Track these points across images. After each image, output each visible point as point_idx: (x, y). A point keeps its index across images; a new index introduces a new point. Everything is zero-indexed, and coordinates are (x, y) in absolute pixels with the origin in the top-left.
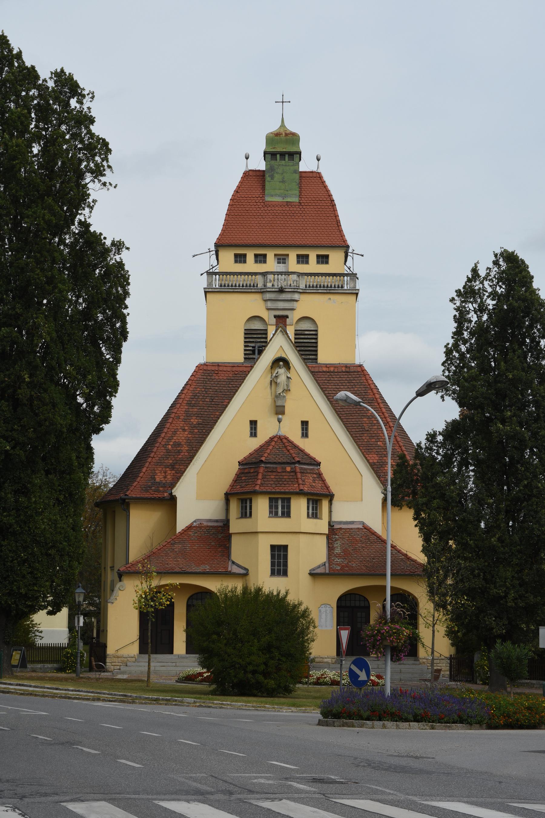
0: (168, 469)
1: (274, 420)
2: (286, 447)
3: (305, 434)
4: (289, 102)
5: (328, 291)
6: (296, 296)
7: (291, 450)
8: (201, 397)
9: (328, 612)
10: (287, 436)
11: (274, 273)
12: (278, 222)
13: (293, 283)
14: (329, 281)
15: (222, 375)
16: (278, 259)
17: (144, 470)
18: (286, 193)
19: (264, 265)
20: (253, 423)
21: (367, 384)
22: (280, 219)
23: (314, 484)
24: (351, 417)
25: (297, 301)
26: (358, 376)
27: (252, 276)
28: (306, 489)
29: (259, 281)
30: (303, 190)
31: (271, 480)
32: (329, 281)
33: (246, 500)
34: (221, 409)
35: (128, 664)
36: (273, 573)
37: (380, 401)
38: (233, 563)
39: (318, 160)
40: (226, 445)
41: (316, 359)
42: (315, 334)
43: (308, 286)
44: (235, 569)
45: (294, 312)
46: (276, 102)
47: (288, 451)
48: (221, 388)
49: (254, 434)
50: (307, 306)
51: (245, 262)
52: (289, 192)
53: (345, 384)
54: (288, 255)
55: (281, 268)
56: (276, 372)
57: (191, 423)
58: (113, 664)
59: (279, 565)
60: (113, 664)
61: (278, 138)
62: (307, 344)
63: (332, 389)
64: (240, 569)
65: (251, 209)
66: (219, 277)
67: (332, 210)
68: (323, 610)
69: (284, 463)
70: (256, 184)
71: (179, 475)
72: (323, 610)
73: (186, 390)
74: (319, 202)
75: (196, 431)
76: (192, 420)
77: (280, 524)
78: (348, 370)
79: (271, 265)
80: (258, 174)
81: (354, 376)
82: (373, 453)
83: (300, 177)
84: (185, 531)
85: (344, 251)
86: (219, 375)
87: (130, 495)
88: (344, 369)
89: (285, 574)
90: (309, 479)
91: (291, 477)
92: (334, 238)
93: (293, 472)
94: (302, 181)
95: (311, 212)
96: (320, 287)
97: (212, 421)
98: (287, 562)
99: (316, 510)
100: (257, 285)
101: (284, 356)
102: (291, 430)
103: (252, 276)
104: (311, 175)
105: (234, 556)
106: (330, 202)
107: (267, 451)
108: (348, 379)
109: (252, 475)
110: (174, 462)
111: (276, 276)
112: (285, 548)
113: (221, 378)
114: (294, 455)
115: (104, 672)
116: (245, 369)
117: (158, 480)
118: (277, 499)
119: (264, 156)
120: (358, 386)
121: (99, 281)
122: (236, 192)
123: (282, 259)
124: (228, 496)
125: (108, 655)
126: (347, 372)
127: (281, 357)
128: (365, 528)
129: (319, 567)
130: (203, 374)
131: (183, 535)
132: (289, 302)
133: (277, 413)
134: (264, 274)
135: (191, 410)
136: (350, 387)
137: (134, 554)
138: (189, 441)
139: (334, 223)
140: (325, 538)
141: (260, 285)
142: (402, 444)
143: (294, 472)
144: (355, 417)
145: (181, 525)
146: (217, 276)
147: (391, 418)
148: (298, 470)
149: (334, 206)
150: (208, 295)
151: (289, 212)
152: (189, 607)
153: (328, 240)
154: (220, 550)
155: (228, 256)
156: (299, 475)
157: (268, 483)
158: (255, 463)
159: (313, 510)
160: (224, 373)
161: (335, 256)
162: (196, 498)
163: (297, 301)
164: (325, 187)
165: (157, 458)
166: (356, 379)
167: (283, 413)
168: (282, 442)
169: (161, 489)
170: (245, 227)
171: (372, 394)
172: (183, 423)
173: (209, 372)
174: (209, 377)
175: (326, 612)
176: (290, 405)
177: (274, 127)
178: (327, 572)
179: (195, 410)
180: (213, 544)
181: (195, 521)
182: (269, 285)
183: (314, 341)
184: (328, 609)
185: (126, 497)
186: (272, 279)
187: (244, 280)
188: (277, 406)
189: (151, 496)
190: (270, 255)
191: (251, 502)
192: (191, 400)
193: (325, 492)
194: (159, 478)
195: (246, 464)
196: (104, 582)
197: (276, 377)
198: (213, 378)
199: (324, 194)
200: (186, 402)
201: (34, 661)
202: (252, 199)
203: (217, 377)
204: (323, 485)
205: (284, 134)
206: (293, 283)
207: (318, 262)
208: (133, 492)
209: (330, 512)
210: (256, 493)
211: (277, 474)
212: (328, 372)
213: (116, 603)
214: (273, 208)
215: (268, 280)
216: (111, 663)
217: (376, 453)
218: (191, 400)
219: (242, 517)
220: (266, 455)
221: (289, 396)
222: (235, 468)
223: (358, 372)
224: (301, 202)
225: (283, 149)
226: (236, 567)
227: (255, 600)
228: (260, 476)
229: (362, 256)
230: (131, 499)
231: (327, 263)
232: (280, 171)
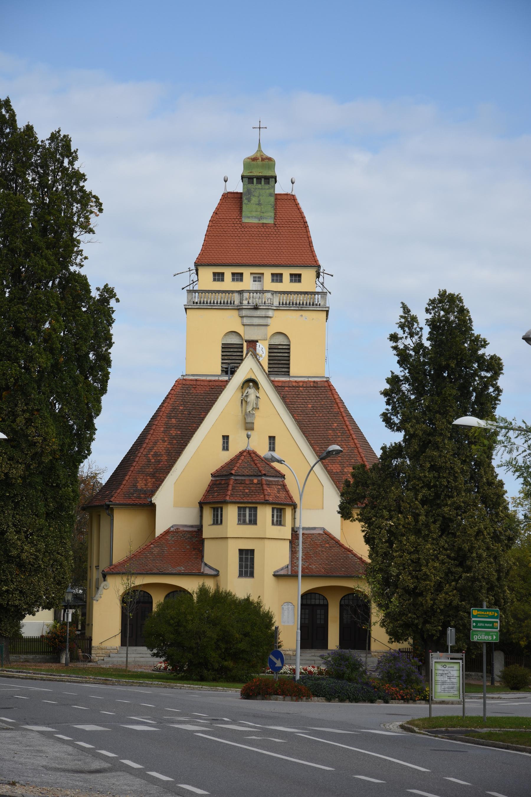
0: (148, 477)
1: (244, 433)
2: (253, 461)
3: (272, 448)
5: (300, 309)
6: (270, 313)
7: (258, 464)
10: (256, 450)
11: (249, 291)
12: (255, 243)
13: (268, 301)
14: (300, 299)
15: (200, 389)
16: (254, 277)
17: (127, 478)
18: (262, 215)
20: (226, 438)
21: (333, 398)
22: (256, 240)
23: (278, 495)
24: (317, 430)
25: (271, 317)
26: (325, 391)
27: (229, 294)
28: (271, 499)
29: (236, 298)
30: (278, 212)
31: (239, 491)
32: (300, 299)
33: (217, 508)
34: (198, 421)
35: (111, 655)
36: (241, 575)
37: (344, 415)
38: (206, 564)
40: (201, 456)
41: (289, 372)
43: (281, 304)
44: (207, 571)
45: (268, 327)
46: (253, 128)
47: (256, 465)
48: (198, 401)
49: (226, 447)
50: (282, 322)
51: (223, 280)
52: (265, 214)
54: (263, 274)
55: (255, 286)
56: (246, 392)
57: (170, 434)
61: (255, 163)
62: (280, 359)
63: (300, 403)
64: (212, 571)
65: (228, 230)
66: (198, 295)
67: (305, 231)
68: (285, 607)
69: (251, 476)
70: (234, 206)
71: (159, 482)
72: (285, 607)
73: (166, 403)
74: (293, 223)
75: (175, 442)
76: (171, 432)
77: (248, 530)
78: (315, 385)
79: (248, 283)
80: (236, 196)
81: (321, 391)
82: (336, 463)
83: (276, 199)
84: (163, 536)
85: (316, 270)
86: (197, 389)
87: (114, 502)
88: (312, 384)
89: (252, 575)
91: (257, 488)
92: (306, 258)
93: (259, 484)
94: (278, 203)
95: (286, 233)
96: (293, 304)
97: (190, 433)
98: (253, 564)
99: (280, 517)
103: (229, 294)
104: (286, 197)
105: (207, 559)
106: (303, 223)
107: (236, 465)
108: (315, 393)
109: (223, 486)
110: (155, 470)
111: (251, 294)
112: (252, 552)
113: (198, 392)
114: (261, 469)
115: (90, 662)
116: (221, 384)
117: (139, 487)
118: (245, 508)
119: (242, 179)
120: (325, 401)
121: (85, 326)
122: (215, 213)
123: (258, 278)
124: (202, 505)
125: (93, 647)
126: (315, 387)
128: (325, 534)
129: (282, 569)
131: (161, 539)
132: (264, 319)
133: (247, 429)
134: (241, 292)
139: (306, 244)
141: (237, 302)
142: (363, 455)
143: (260, 483)
144: (321, 430)
145: (160, 530)
146: (197, 294)
147: (354, 430)
148: (264, 482)
149: (306, 227)
150: (188, 310)
151: (265, 233)
152: (342, 608)
153: (301, 260)
154: (194, 553)
155: (207, 273)
156: (265, 487)
157: (237, 493)
158: (226, 475)
159: (277, 518)
160: (201, 387)
161: (308, 275)
162: (173, 504)
163: (271, 317)
164: (299, 209)
166: (323, 393)
167: (252, 429)
168: (251, 456)
169: (142, 496)
170: (223, 247)
171: (337, 408)
173: (187, 386)
174: (187, 391)
175: (288, 610)
176: (258, 422)
177: (251, 152)
178: (290, 573)
180: (188, 547)
181: (172, 527)
182: (245, 302)
183: (286, 355)
184: (290, 607)
185: (110, 503)
186: (248, 297)
187: (222, 298)
189: (133, 502)
190: (247, 272)
191: (222, 511)
192: (170, 412)
194: (141, 485)
195: (218, 476)
196: (90, 579)
197: (247, 396)
198: (191, 392)
199: (298, 216)
200: (166, 414)
203: (195, 391)
204: (287, 495)
205: (260, 159)
206: (268, 301)
207: (291, 281)
208: (117, 498)
209: (294, 519)
210: (226, 503)
211: (246, 484)
212: (297, 387)
213: (100, 600)
214: (250, 230)
215: (244, 298)
217: (340, 463)
218: (170, 412)
219: (214, 524)
221: (257, 413)
222: (210, 478)
223: (325, 387)
224: (276, 223)
225: (259, 174)
226: (208, 568)
227: (221, 600)
228: (230, 488)
229: (332, 276)
231: (300, 281)
232: (257, 194)
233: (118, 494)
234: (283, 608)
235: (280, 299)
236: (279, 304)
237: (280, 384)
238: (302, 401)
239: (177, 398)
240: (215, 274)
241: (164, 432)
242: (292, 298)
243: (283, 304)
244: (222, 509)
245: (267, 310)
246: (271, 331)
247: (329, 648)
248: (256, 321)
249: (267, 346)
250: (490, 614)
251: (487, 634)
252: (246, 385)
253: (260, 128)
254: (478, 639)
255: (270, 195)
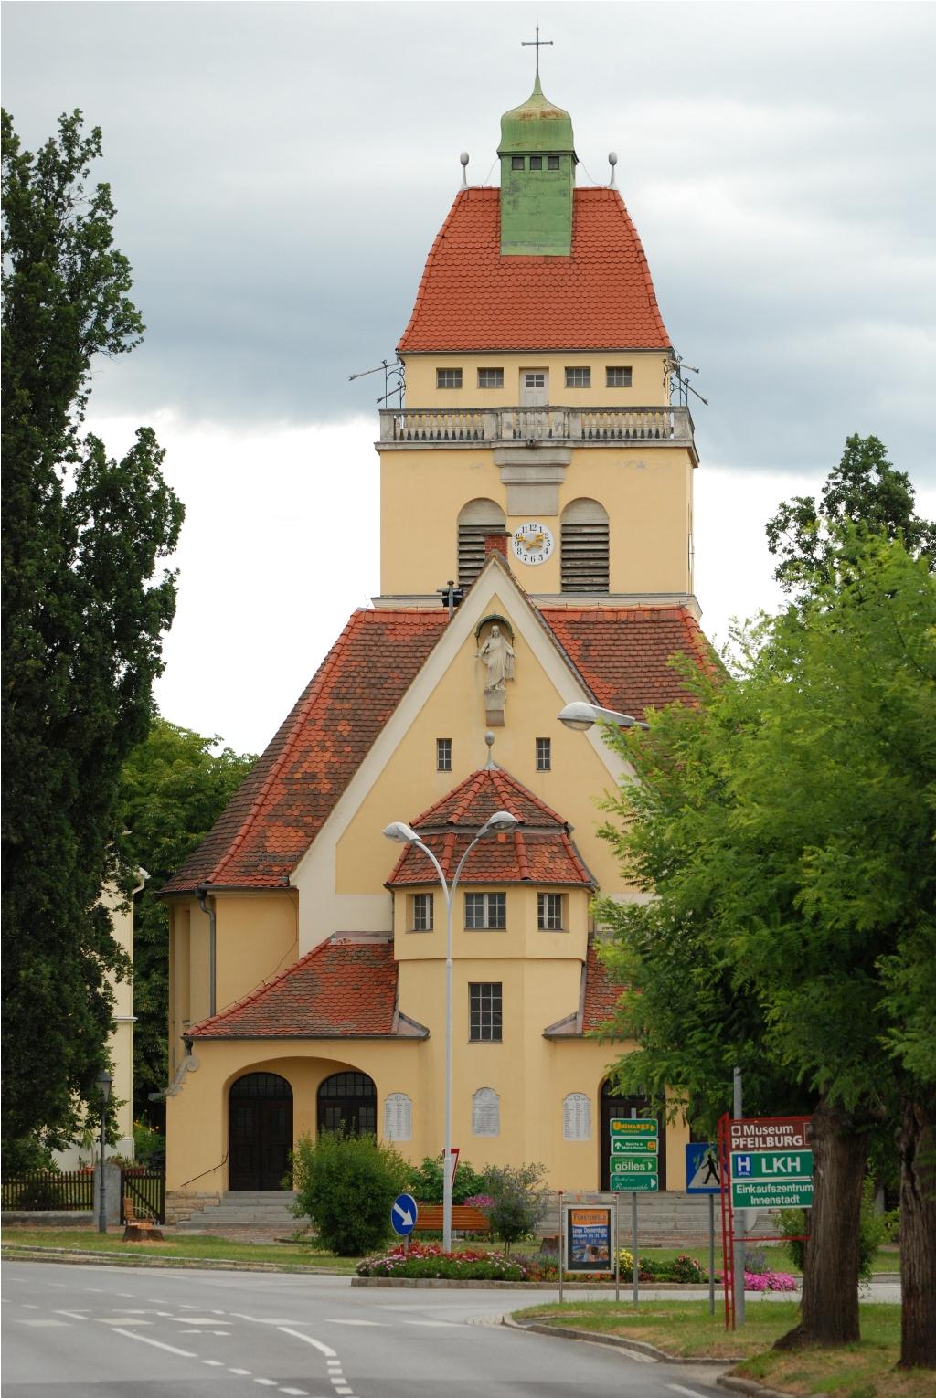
4: (552, 43)
5: (629, 445)
6: (563, 456)
8: (358, 680)
9: (581, 1108)
13: (557, 430)
15: (403, 632)
16: (529, 377)
19: (497, 392)
20: (444, 744)
23: (551, 866)
28: (534, 876)
36: (474, 1036)
38: (402, 1016)
39: (613, 163)
40: (393, 785)
42: (601, 535)
43: (587, 434)
45: (562, 486)
48: (398, 660)
49: (445, 765)
50: (592, 475)
51: (459, 385)
53: (647, 647)
54: (547, 369)
56: (486, 645)
57: (337, 733)
58: (177, 1210)
59: (486, 1020)
60: (177, 1210)
62: (585, 557)
63: (621, 659)
66: (406, 420)
72: (571, 1104)
76: (339, 728)
77: (487, 942)
78: (655, 617)
80: (487, 196)
83: (575, 201)
87: (215, 883)
88: (647, 616)
90: (544, 855)
94: (580, 209)
100: (483, 433)
101: (500, 613)
102: (516, 760)
113: (399, 638)
118: (480, 896)
123: (535, 378)
126: (654, 622)
127: (495, 616)
129: (564, 1022)
130: (364, 632)
132: (548, 469)
135: (338, 707)
136: (657, 653)
137: (228, 998)
138: (333, 771)
140: (578, 967)
151: (551, 278)
155: (423, 373)
156: (522, 849)
159: (551, 913)
161: (647, 370)
164: (627, 221)
165: (271, 807)
167: (500, 724)
172: (323, 733)
173: (375, 627)
174: (376, 638)
176: (517, 704)
177: (517, 99)
179: (347, 706)
181: (334, 936)
185: (208, 886)
188: (488, 711)
193: (575, 880)
194: (273, 845)
198: (384, 638)
200: (329, 690)
201: (84, 1205)
202: (474, 251)
203: (392, 638)
204: (571, 866)
206: (557, 430)
207: (610, 384)
212: (616, 623)
215: (505, 425)
216: (174, 1208)
219: (417, 930)
220: (459, 811)
225: (538, 146)
226: (406, 1024)
230: (217, 890)
231: (628, 384)
233: (225, 865)
234: (566, 1106)
235: (583, 425)
236: (583, 437)
237: (577, 618)
238: (624, 653)
239: (354, 653)
240: (441, 372)
241: (325, 729)
242: (610, 421)
243: (590, 436)
244: (431, 896)
245: (556, 451)
246: (566, 495)
247: (668, 1188)
248: (532, 475)
249: (558, 530)
250: (643, 1128)
251: (638, 1160)
252: (484, 630)
253: (537, 44)
254: (622, 1171)
255: (563, 193)
